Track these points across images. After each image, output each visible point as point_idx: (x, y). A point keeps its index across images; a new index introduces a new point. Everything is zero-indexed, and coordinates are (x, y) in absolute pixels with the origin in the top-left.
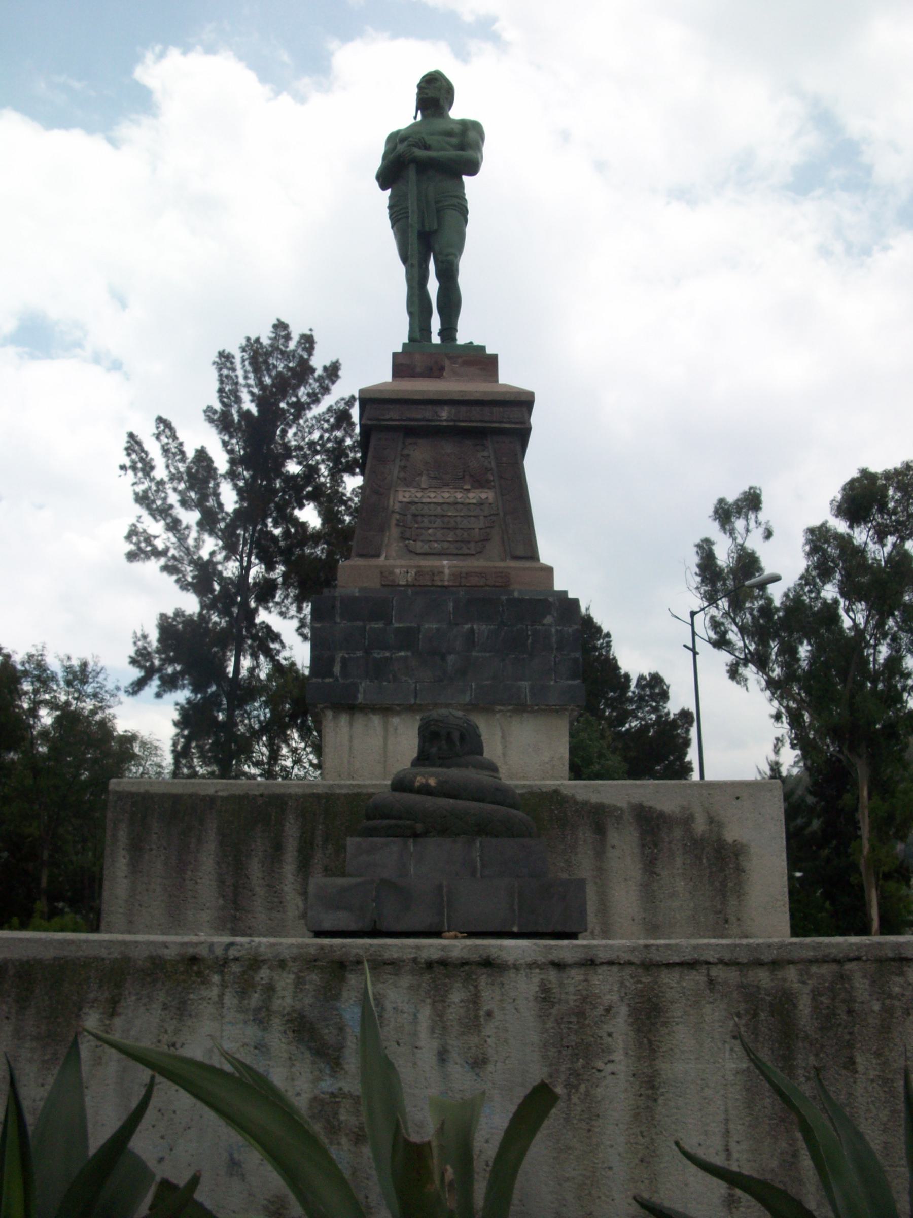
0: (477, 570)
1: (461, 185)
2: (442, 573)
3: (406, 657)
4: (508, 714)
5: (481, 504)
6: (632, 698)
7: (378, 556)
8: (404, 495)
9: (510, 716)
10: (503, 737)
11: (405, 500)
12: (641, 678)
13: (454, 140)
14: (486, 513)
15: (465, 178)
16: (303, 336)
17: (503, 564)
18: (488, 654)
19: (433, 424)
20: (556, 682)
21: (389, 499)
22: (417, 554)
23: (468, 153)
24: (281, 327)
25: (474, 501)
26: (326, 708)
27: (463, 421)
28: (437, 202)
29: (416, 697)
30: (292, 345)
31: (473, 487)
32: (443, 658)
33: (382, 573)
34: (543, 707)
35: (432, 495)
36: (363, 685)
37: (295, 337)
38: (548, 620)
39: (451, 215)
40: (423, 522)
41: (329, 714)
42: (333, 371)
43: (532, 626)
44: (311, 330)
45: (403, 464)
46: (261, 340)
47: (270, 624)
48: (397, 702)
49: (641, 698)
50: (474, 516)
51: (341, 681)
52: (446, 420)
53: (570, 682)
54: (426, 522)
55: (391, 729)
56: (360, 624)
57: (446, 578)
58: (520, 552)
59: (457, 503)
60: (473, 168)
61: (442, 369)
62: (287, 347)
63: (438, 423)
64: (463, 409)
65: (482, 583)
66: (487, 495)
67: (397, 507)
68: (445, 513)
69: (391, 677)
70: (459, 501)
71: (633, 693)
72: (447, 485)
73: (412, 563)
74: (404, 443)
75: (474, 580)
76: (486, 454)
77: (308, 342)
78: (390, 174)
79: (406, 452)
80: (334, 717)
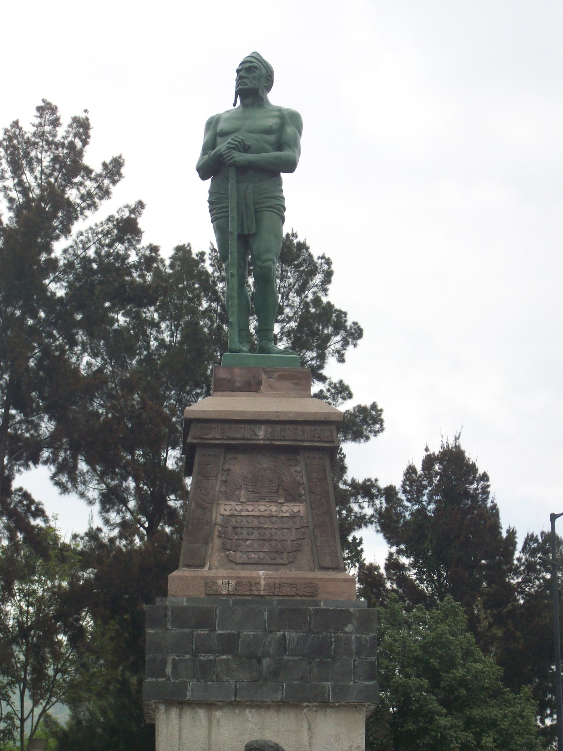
0: (288, 581)
1: (279, 183)
2: (259, 583)
3: (228, 660)
4: (314, 709)
5: (293, 517)
6: (518, 567)
7: (203, 566)
8: (225, 508)
9: (316, 711)
10: (309, 729)
11: (226, 513)
12: (530, 539)
13: (272, 138)
14: (298, 526)
15: (282, 175)
16: (75, 120)
17: (311, 575)
18: (297, 658)
19: (251, 442)
20: (355, 682)
21: (212, 514)
22: (237, 564)
24: (46, 109)
25: (287, 514)
26: (159, 703)
27: (278, 440)
28: (254, 204)
29: (236, 695)
30: (61, 132)
31: (287, 501)
32: (259, 661)
33: (206, 583)
34: (344, 703)
35: (250, 508)
36: (192, 684)
37: (65, 120)
38: (349, 628)
39: (268, 217)
40: (242, 533)
41: (162, 708)
42: (114, 170)
43: (335, 633)
44: (86, 111)
45: (224, 478)
46: (20, 124)
47: (29, 491)
48: (219, 700)
49: (530, 567)
50: (287, 529)
51: (173, 680)
53: (368, 683)
54: (245, 536)
55: (214, 722)
56: (187, 630)
57: (262, 588)
58: (327, 562)
59: (272, 516)
60: (290, 166)
61: (260, 383)
62: (55, 136)
63: (255, 442)
64: (278, 428)
65: (293, 593)
66: (299, 508)
67: (219, 520)
68: (261, 526)
69: (214, 677)
70: (274, 514)
71: (519, 559)
72: (263, 498)
73: (232, 573)
74: (225, 458)
75: (286, 590)
76: (298, 468)
77: (82, 126)
78: (211, 167)
79: (227, 466)
80: (167, 710)
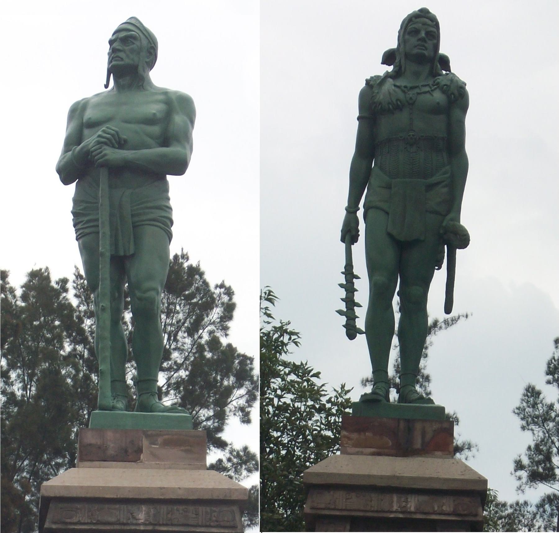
1: (165, 189)
13: (156, 129)
15: (169, 178)
19: (128, 528)
23: (173, 150)
27: (163, 525)
28: (133, 216)
39: (150, 233)
52: (144, 524)
60: (179, 167)
61: (140, 451)
63: (133, 527)
64: (164, 509)
